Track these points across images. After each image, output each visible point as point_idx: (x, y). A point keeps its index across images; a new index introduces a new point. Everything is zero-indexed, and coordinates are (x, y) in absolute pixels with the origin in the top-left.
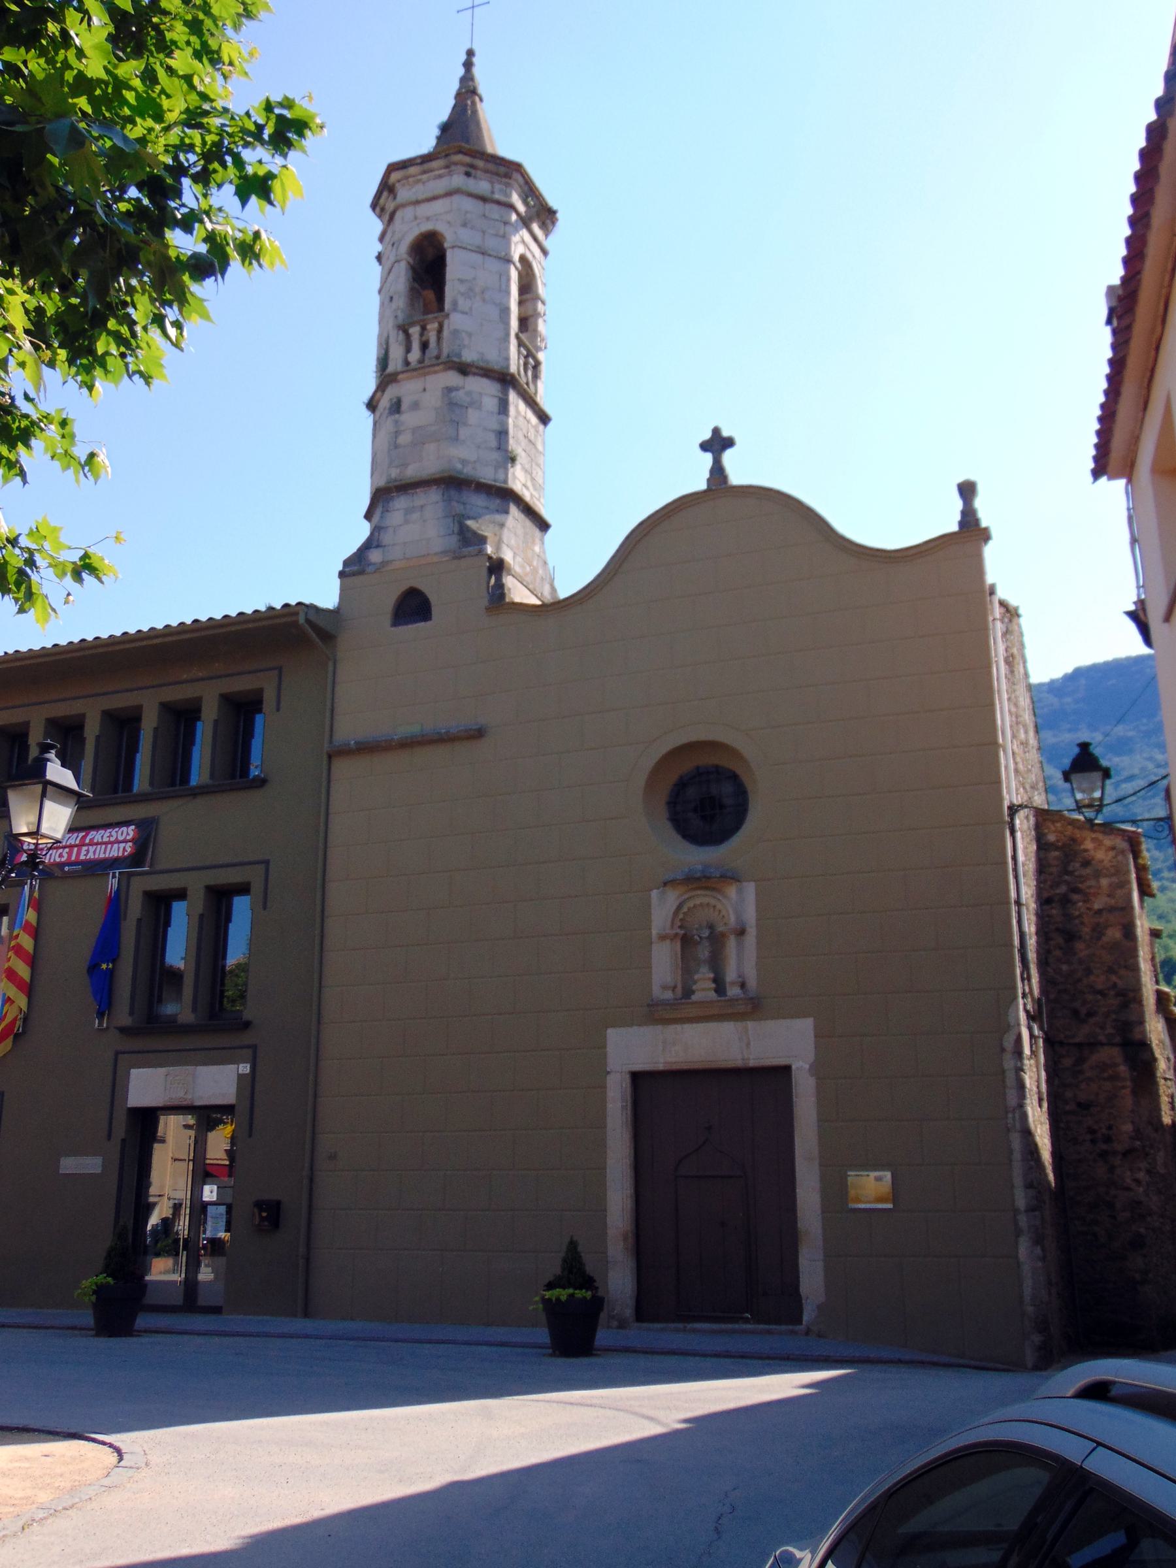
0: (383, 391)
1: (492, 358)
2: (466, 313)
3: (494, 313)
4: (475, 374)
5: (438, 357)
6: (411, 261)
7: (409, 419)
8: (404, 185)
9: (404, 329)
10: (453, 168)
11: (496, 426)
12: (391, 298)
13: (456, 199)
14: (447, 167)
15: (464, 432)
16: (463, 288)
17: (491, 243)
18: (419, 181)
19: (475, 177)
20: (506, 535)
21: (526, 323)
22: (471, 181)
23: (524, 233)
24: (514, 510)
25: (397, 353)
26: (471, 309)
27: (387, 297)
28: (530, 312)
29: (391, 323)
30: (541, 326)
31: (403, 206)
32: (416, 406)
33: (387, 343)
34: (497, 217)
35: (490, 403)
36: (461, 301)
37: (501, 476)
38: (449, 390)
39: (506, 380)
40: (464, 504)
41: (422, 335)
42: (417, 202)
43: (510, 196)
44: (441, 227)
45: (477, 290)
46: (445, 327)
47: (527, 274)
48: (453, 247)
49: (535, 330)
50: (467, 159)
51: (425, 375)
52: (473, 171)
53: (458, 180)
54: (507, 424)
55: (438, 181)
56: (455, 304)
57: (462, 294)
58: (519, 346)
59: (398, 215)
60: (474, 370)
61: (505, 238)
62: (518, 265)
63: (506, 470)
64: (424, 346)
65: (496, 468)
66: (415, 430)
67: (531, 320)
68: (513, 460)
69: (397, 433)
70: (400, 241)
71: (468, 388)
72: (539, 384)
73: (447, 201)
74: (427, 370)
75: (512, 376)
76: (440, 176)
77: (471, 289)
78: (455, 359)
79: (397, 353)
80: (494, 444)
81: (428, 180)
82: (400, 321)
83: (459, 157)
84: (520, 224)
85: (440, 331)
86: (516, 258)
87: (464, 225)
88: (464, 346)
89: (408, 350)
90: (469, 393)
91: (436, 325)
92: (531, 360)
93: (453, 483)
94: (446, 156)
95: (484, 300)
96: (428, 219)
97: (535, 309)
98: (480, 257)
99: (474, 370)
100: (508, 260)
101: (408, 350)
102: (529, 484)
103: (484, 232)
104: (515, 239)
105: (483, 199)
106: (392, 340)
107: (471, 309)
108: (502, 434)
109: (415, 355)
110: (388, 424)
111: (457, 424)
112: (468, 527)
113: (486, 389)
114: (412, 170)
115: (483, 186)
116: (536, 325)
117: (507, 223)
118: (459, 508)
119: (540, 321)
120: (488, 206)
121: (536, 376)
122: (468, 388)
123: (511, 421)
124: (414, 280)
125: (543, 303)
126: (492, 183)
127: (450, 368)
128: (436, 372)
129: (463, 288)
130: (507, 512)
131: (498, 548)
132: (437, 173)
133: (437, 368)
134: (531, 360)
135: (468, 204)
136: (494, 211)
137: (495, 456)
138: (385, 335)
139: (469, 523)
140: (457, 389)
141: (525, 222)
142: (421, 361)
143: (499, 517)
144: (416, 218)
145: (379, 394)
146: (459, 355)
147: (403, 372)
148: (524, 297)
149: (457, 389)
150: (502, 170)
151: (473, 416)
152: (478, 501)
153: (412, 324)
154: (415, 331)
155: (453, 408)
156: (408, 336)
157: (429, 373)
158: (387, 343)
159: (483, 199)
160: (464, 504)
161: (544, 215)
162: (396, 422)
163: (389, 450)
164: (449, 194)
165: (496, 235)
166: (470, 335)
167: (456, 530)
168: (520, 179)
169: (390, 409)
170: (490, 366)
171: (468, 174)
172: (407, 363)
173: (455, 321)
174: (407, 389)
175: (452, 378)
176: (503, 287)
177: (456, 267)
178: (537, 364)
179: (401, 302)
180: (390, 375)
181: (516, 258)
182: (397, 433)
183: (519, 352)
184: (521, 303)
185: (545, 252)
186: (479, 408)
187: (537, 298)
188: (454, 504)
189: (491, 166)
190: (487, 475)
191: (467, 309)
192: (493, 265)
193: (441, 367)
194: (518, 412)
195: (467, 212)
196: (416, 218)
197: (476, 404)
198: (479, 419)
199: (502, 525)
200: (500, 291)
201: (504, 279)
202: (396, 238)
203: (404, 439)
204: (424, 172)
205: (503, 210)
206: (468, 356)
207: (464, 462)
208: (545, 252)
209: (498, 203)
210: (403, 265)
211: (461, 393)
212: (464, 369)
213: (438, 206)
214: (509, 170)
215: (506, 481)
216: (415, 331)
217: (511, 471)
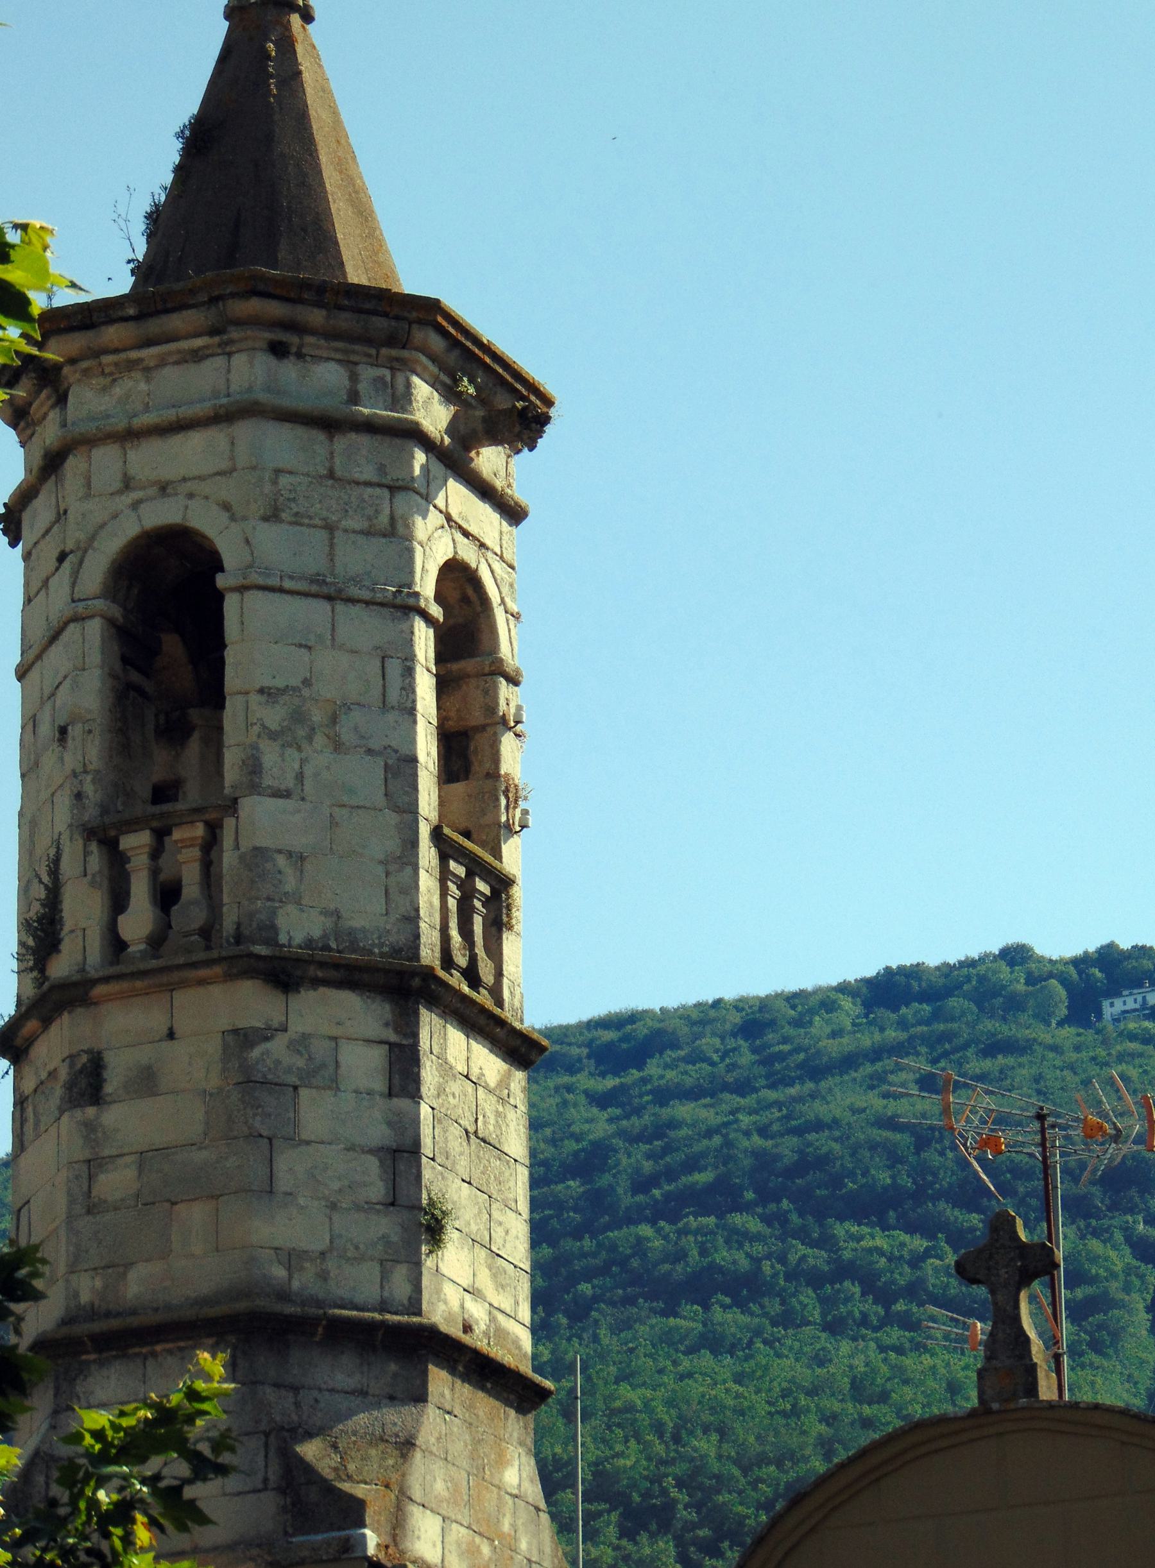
0: (47, 1022)
1: (366, 915)
2: (286, 794)
3: (366, 776)
4: (316, 983)
5: (206, 932)
6: (116, 612)
7: (126, 1121)
8: (86, 372)
9: (103, 836)
10: (234, 334)
11: (379, 1134)
12: (63, 731)
13: (245, 430)
14: (213, 332)
15: (290, 1166)
16: (274, 717)
17: (356, 559)
18: (132, 365)
19: (300, 356)
20: (430, 1476)
21: (468, 749)
22: (288, 371)
23: (456, 496)
24: (441, 1383)
25: (83, 908)
26: (300, 777)
27: (44, 735)
28: (476, 717)
29: (62, 816)
30: (513, 757)
31: (89, 442)
32: (146, 1082)
33: (54, 870)
34: (367, 473)
35: (364, 1064)
36: (270, 756)
37: (400, 1289)
38: (243, 1039)
39: (405, 987)
40: (295, 1389)
41: (156, 853)
42: (130, 436)
43: (402, 399)
44: (205, 520)
45: (317, 716)
46: (228, 841)
47: (465, 599)
48: (242, 589)
49: (494, 775)
50: (275, 309)
51: (171, 988)
52: (293, 339)
53: (248, 371)
54: (416, 1121)
55: (192, 369)
56: (253, 767)
57: (273, 736)
58: (444, 858)
59: (74, 465)
60: (313, 971)
61: (397, 537)
62: (436, 611)
63: (416, 1265)
64: (167, 896)
65: (385, 1267)
66: (144, 1158)
67: (480, 741)
68: (434, 1232)
69: (93, 1165)
70: (84, 549)
71: (297, 1027)
72: (511, 946)
73: (217, 436)
74: (176, 976)
75: (428, 973)
76: (197, 356)
77: (298, 717)
78: (261, 950)
79: (83, 908)
80: (377, 1190)
81: (162, 363)
82: (91, 814)
83: (254, 306)
84: (438, 468)
85: (211, 843)
86: (426, 585)
87: (272, 516)
88: (286, 898)
89: (119, 902)
90: (301, 1043)
91: (199, 830)
92: (482, 886)
93: (268, 1328)
94: (214, 300)
95: (338, 746)
96: (164, 488)
97: (491, 708)
98: (324, 606)
99: (313, 971)
100: (406, 607)
101: (119, 902)
102: (485, 1281)
103: (330, 528)
104: (426, 526)
105: (329, 424)
106: (68, 867)
107: (300, 777)
108: (402, 1155)
109: (137, 922)
110: (63, 1136)
111: (270, 1144)
112: (308, 1469)
113: (357, 1016)
114: (112, 334)
115: (322, 379)
116: (496, 759)
117: (399, 487)
118: (280, 1405)
119: (508, 743)
120: (342, 442)
121: (498, 924)
122: (297, 1027)
123: (425, 1110)
124: (125, 660)
125: (514, 681)
126: (350, 364)
127: (248, 973)
128: (202, 982)
129: (274, 717)
130: (420, 1397)
131: (397, 1526)
132: (185, 345)
133: (203, 973)
134: (482, 886)
135: (281, 445)
136: (359, 457)
137: (385, 1225)
138: (44, 845)
139: (310, 1450)
140: (265, 1034)
141: (454, 460)
142: (157, 941)
143: (394, 1417)
144: (128, 483)
145: (32, 1025)
146: (269, 932)
147: (106, 980)
148: (455, 667)
149: (265, 1034)
150: (380, 324)
151: (315, 1112)
152: (338, 1373)
153: (131, 825)
154: (136, 843)
155: (256, 1095)
156: (117, 861)
157: (183, 984)
158: (54, 870)
159: (329, 424)
160: (295, 1389)
161: (511, 409)
162: (90, 1127)
163: (70, 1218)
164: (225, 416)
165: (367, 533)
166: (298, 859)
167: (274, 1473)
168: (436, 342)
169: (70, 1086)
170: (408, 1477)
171: (278, 350)
172: (116, 945)
173: (261, 821)
174: (123, 1028)
175: (252, 1003)
176: (393, 696)
177: (259, 640)
178: (502, 884)
179: (90, 749)
180: (63, 986)
181: (426, 585)
182: (93, 1165)
183: (444, 875)
184: (444, 685)
185: (513, 513)
186: (334, 1085)
187: (499, 671)
188: (269, 1394)
189: (345, 321)
190: (358, 1287)
191: (289, 782)
192: (361, 627)
193: (218, 970)
194: (446, 1069)
195: (278, 472)
196: (128, 483)
197: (324, 1075)
198: (332, 1121)
199: (406, 1446)
200: (385, 706)
201: (394, 668)
202: (74, 535)
203: (116, 1182)
204: (149, 343)
205: (384, 447)
206: (298, 927)
207: (292, 1258)
208: (513, 513)
209: (370, 427)
210: (95, 627)
211: (277, 1047)
212: (285, 973)
213: (193, 452)
214: (409, 327)
215: (415, 1307)
216: (136, 843)
217: (429, 1263)
